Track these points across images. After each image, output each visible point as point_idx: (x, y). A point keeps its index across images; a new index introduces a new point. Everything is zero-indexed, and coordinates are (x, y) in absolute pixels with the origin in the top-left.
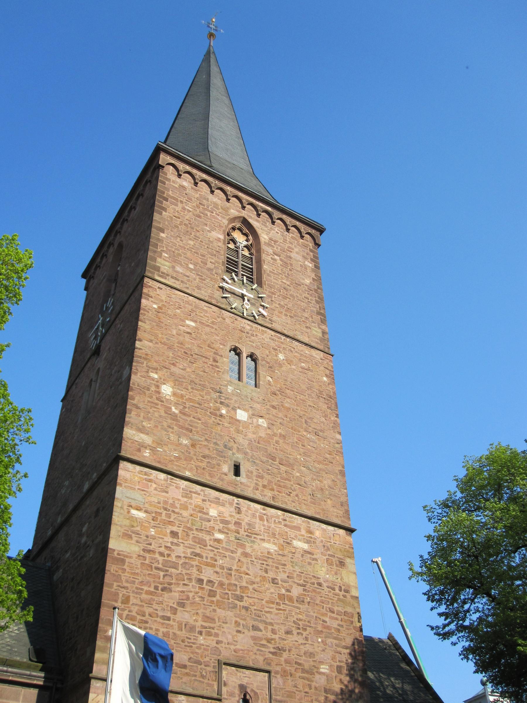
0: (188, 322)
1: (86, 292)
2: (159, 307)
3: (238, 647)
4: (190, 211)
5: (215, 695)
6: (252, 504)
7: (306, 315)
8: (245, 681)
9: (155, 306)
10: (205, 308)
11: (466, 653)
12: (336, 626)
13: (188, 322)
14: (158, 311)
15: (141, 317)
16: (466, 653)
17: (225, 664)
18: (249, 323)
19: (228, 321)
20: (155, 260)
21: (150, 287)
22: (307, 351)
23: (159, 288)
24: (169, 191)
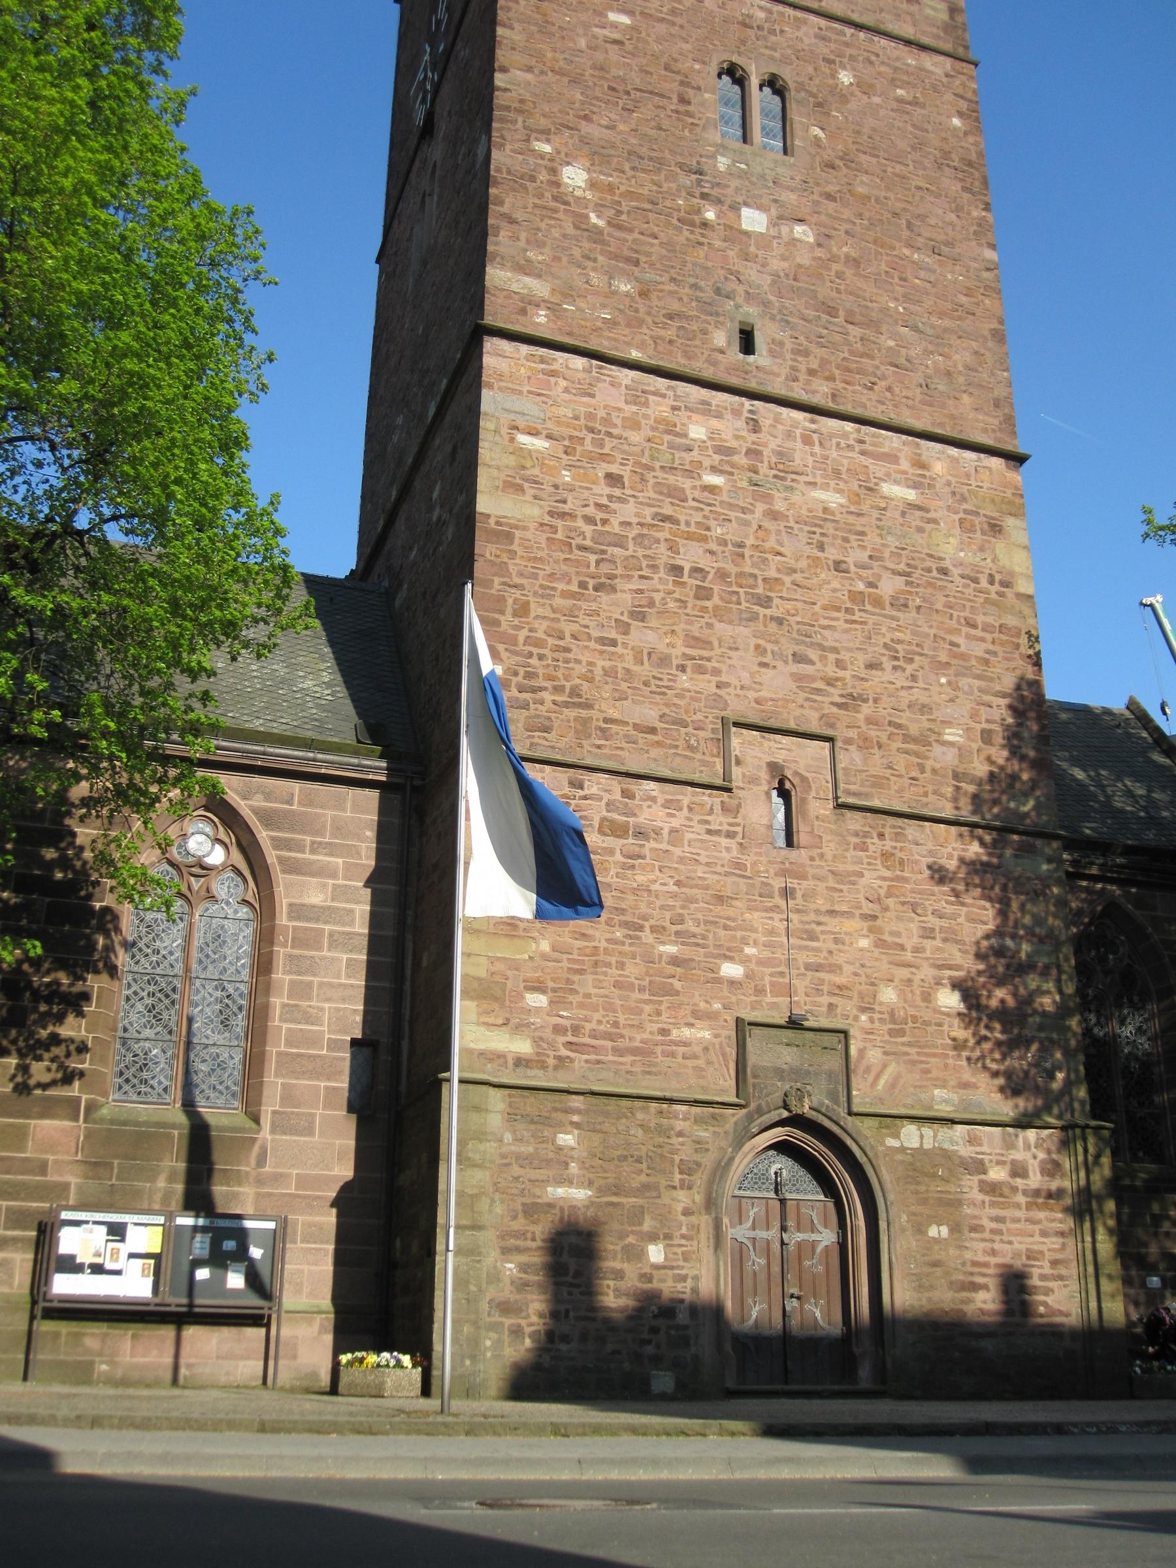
3: (764, 694)
5: (719, 782)
8: (779, 758)
17: (736, 724)
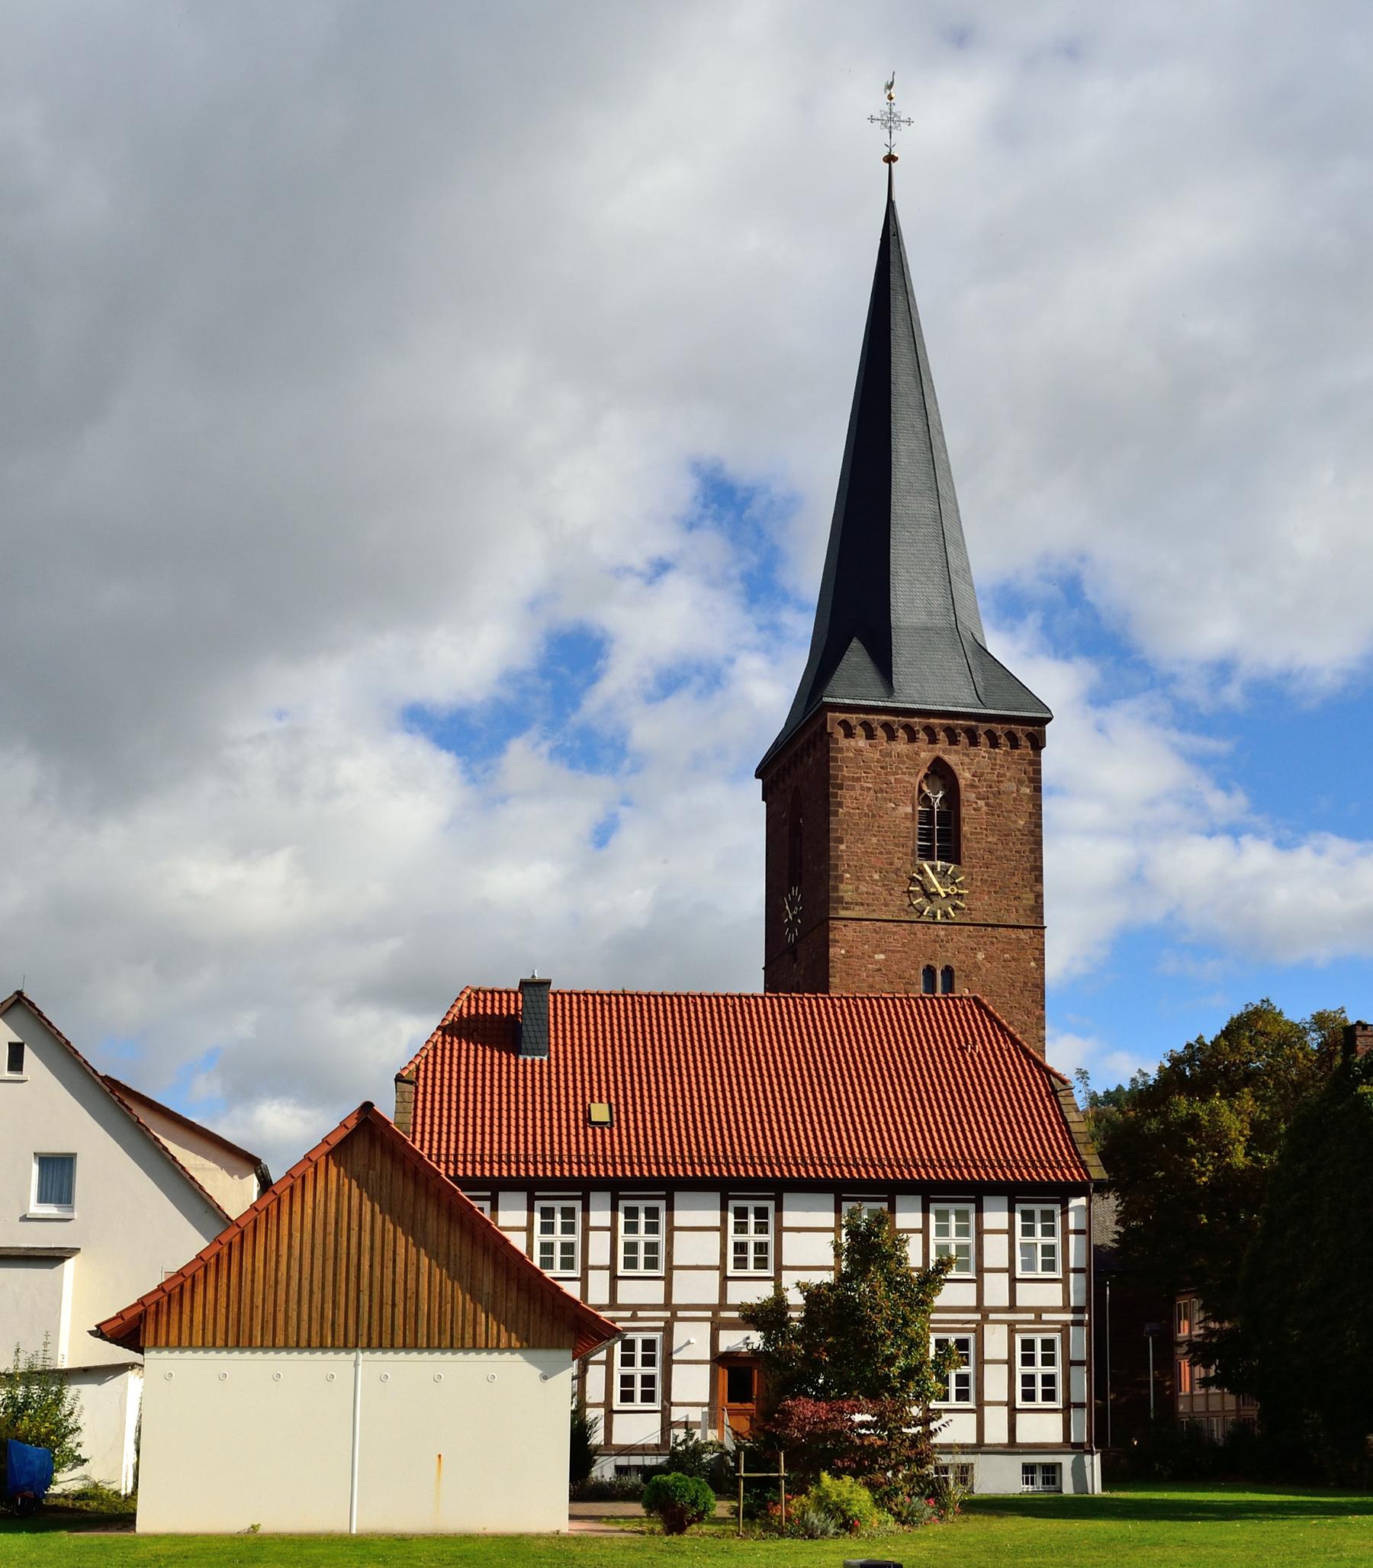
0: (877, 957)
1: (760, 781)
2: (847, 951)
4: (870, 789)
6: (891, 918)
7: (1015, 879)
9: (843, 952)
10: (894, 929)
11: (1120, 1088)
12: (899, 808)
13: (877, 957)
14: (848, 955)
15: (831, 971)
16: (1120, 1088)
18: (944, 926)
19: (920, 935)
20: (836, 889)
21: (835, 928)
22: (1013, 934)
23: (845, 926)
24: (842, 771)
